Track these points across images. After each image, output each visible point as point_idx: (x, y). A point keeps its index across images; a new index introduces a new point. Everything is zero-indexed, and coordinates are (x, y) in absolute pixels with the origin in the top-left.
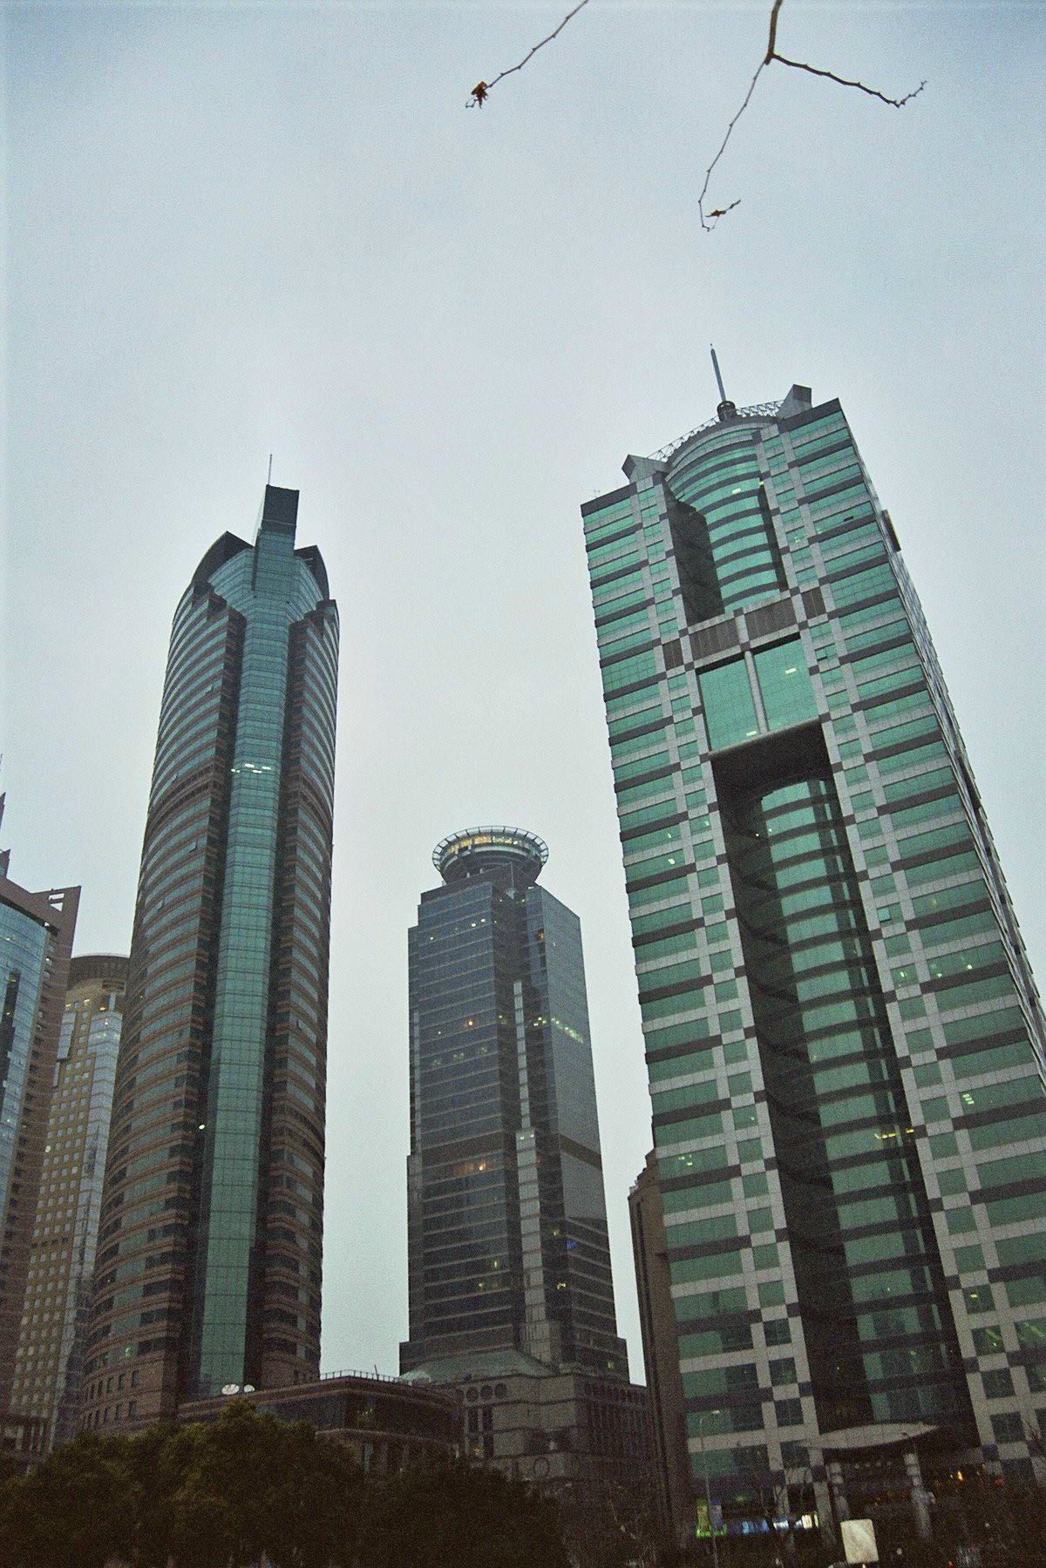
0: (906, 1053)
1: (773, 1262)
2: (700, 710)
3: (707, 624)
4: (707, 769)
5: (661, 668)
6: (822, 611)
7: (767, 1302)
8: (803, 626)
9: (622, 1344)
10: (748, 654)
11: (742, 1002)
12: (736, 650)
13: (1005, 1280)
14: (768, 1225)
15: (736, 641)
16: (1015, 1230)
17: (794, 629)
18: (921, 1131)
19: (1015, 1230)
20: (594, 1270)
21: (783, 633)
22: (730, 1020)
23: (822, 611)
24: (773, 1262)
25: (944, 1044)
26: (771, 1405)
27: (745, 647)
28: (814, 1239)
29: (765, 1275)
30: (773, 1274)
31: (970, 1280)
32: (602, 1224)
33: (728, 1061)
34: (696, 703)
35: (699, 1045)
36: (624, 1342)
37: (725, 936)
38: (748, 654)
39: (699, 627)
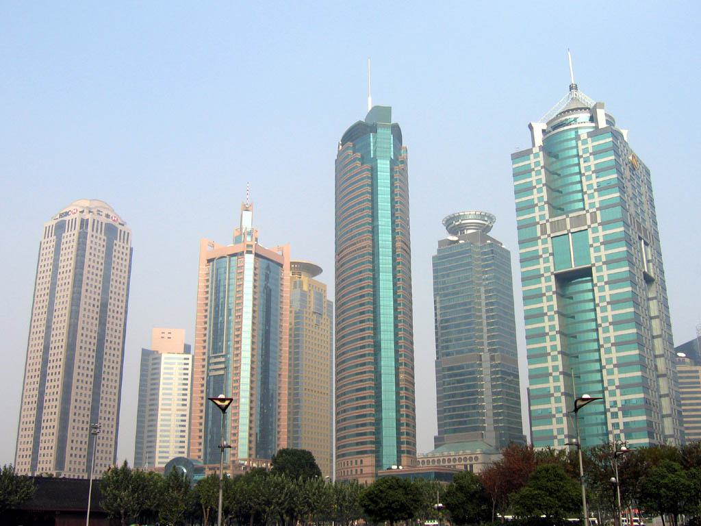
0: (605, 364)
1: (553, 320)
2: (552, 254)
3: (556, 219)
4: (553, 278)
5: (539, 234)
6: (596, 222)
7: (552, 350)
8: (589, 227)
9: (525, 437)
10: (570, 234)
11: (543, 176)
12: (566, 232)
13: (605, 244)
14: (558, 370)
15: (566, 228)
16: (617, 312)
17: (586, 227)
18: (594, 265)
19: (617, 312)
20: (517, 398)
21: (583, 228)
22: (540, 199)
23: (596, 222)
24: (553, 320)
25: (609, 300)
26: (539, 226)
27: (569, 231)
28: (570, 355)
29: (559, 426)
30: (558, 384)
31: (606, 346)
32: (518, 397)
33: (534, 158)
34: (551, 251)
35: (530, 207)
36: (508, 252)
37: (540, 174)
38: (570, 234)
39: (553, 219)
